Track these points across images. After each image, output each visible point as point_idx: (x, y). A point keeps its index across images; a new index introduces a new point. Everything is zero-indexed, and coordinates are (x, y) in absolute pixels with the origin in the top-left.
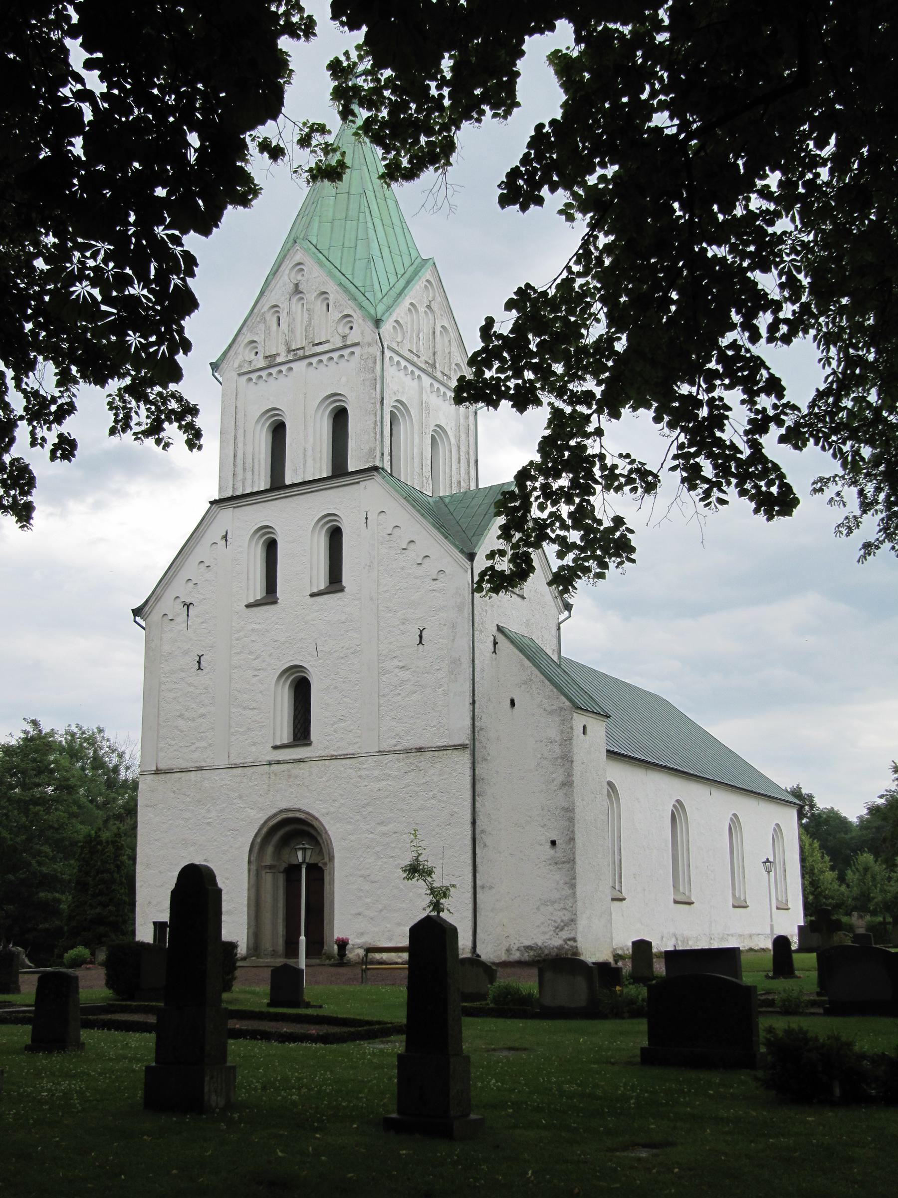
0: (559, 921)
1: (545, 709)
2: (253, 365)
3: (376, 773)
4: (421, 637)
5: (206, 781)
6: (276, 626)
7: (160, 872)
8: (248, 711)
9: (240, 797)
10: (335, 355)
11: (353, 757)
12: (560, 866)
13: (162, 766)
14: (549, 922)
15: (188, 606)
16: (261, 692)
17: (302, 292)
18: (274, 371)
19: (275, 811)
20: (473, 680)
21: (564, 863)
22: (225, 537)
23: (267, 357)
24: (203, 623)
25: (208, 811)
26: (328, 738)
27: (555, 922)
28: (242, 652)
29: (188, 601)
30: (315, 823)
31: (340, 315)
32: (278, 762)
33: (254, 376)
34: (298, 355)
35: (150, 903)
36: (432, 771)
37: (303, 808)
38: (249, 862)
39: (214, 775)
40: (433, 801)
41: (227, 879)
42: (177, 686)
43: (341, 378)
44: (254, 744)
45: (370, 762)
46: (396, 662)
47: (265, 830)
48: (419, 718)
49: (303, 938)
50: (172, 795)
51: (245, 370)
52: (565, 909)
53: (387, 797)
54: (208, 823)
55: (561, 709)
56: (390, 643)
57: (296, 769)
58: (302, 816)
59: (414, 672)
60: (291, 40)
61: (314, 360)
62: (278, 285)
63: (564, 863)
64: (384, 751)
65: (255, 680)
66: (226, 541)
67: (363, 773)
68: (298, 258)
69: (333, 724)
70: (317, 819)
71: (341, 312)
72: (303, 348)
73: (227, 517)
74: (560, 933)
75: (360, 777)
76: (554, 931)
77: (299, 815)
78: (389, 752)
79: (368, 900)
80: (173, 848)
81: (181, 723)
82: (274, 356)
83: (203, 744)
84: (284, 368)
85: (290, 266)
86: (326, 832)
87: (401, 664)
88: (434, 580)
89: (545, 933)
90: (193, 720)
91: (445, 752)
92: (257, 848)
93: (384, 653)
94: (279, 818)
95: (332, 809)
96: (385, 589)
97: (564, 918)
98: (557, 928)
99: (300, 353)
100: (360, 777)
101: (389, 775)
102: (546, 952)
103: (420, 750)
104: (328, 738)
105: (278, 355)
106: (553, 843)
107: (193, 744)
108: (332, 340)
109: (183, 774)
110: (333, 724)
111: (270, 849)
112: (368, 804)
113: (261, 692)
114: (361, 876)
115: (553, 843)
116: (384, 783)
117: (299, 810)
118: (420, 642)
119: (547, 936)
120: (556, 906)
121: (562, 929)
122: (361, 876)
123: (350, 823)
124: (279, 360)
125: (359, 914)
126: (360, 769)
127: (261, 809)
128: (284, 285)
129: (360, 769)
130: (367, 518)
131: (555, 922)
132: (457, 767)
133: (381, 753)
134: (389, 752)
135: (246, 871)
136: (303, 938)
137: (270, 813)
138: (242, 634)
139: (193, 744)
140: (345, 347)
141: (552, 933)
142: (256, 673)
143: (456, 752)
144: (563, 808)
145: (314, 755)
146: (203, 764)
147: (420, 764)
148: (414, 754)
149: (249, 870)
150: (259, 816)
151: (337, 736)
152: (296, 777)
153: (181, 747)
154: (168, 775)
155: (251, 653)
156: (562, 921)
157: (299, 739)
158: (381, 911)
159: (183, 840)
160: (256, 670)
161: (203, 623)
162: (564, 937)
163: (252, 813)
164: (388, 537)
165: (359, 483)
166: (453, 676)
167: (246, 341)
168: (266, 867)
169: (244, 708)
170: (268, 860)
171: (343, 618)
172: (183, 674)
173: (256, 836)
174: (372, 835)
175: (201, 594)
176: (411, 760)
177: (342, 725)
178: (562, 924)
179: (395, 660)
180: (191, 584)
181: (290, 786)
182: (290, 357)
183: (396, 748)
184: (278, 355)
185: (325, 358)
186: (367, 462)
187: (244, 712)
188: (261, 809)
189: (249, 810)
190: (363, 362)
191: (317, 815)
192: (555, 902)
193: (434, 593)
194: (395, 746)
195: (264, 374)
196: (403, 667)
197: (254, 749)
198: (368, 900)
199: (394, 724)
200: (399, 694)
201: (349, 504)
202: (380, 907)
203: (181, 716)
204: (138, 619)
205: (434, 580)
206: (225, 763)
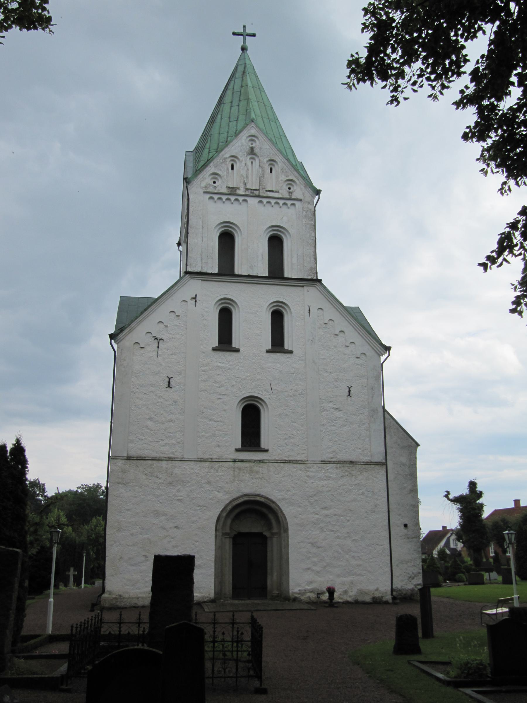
0: (411, 573)
1: (399, 445)
2: (217, 189)
3: (320, 475)
4: (349, 391)
5: (176, 469)
6: (238, 367)
7: (132, 535)
8: (213, 423)
9: (209, 483)
10: (281, 202)
11: (302, 462)
12: (410, 540)
13: (133, 453)
14: (405, 574)
15: (158, 340)
16: (225, 410)
17: (255, 154)
18: (233, 198)
19: (239, 495)
21: (413, 538)
22: (195, 298)
23: (229, 187)
24: (172, 354)
25: (178, 491)
26: (281, 448)
27: (408, 574)
28: (207, 380)
29: (159, 337)
30: (272, 505)
31: (287, 178)
32: (242, 461)
33: (216, 197)
34: (254, 194)
35: (121, 558)
36: (360, 477)
37: (263, 494)
38: (216, 530)
39: (185, 465)
40: (362, 496)
41: (197, 541)
42: (146, 396)
43: (284, 217)
44: (219, 446)
45: (315, 468)
46: (331, 405)
47: (230, 507)
48: (349, 442)
49: (83, 578)
50: (144, 477)
51: (209, 190)
52: (415, 566)
53: (329, 491)
54: (179, 500)
55: (409, 446)
56: (328, 392)
57: (257, 467)
58: (262, 500)
59: (345, 413)
61: (265, 201)
62: (237, 144)
63: (413, 538)
64: (324, 461)
65: (218, 401)
66: (196, 301)
67: (311, 474)
68: (253, 131)
69: (285, 439)
70: (273, 502)
71: (287, 176)
72: (259, 190)
73: (195, 286)
74: (412, 581)
75: (308, 476)
76: (408, 580)
77: (259, 499)
78: (330, 462)
79: (315, 559)
80: (144, 516)
81: (150, 423)
82: (235, 189)
83: (172, 441)
84: (241, 199)
85: (247, 135)
86: (282, 512)
87: (335, 406)
88: (358, 358)
89: (402, 581)
90: (163, 423)
91: (370, 466)
92: (222, 520)
93: (323, 398)
94: (241, 500)
96: (323, 357)
97: (413, 571)
98: (410, 577)
99: (257, 193)
100: (308, 476)
101: (330, 477)
102: (404, 592)
103: (352, 463)
104: (281, 448)
105: (239, 188)
106: (406, 526)
107: (163, 440)
108: (280, 191)
109: (155, 462)
110: (285, 439)
111: (229, 521)
112: (315, 495)
113: (225, 410)
114: (310, 543)
115: (406, 526)
116: (326, 482)
117: (259, 496)
118: (349, 395)
119: (404, 583)
120: (409, 564)
121: (413, 578)
122: (310, 543)
123: (300, 506)
124: (238, 192)
125: (308, 569)
126: (308, 471)
127: (227, 493)
128: (242, 145)
129: (308, 471)
130: (309, 310)
131: (408, 574)
132: (378, 476)
133: (323, 462)
134: (330, 462)
135: (214, 537)
136: (83, 578)
138: (207, 368)
139: (163, 440)
140: (290, 199)
141: (407, 580)
142: (220, 397)
143: (377, 467)
144: (411, 505)
145: (270, 458)
146: (173, 456)
147: (352, 472)
148: (348, 465)
149: (216, 536)
150: (226, 497)
151: (287, 447)
152: (257, 472)
153: (151, 442)
154: (140, 462)
155: (216, 382)
156: (413, 573)
157: (245, 446)
158: (325, 567)
159: (156, 511)
160: (220, 394)
161: (172, 354)
162: (414, 583)
163: (219, 495)
164: (324, 326)
165: (303, 286)
166: (373, 419)
167: (211, 172)
169: (210, 420)
170: (228, 530)
171: (292, 371)
172: (153, 389)
173: (222, 511)
174: (317, 516)
175: (171, 334)
176: (346, 469)
177: (292, 440)
178: (413, 575)
179: (331, 403)
180: (162, 326)
181: (252, 478)
182: (248, 193)
183: (332, 460)
184: (239, 188)
185: (273, 201)
186: (309, 275)
187: (210, 423)
188: (227, 493)
189: (217, 493)
190: (304, 212)
191: (274, 500)
192: (408, 562)
193: (357, 366)
194: (332, 458)
195: (224, 198)
196: (337, 409)
197: (218, 449)
198: (315, 559)
199: (331, 444)
200: (334, 425)
201: (294, 299)
202: (325, 564)
203: (151, 419)
204: (113, 341)
205: (358, 358)
206: (194, 457)
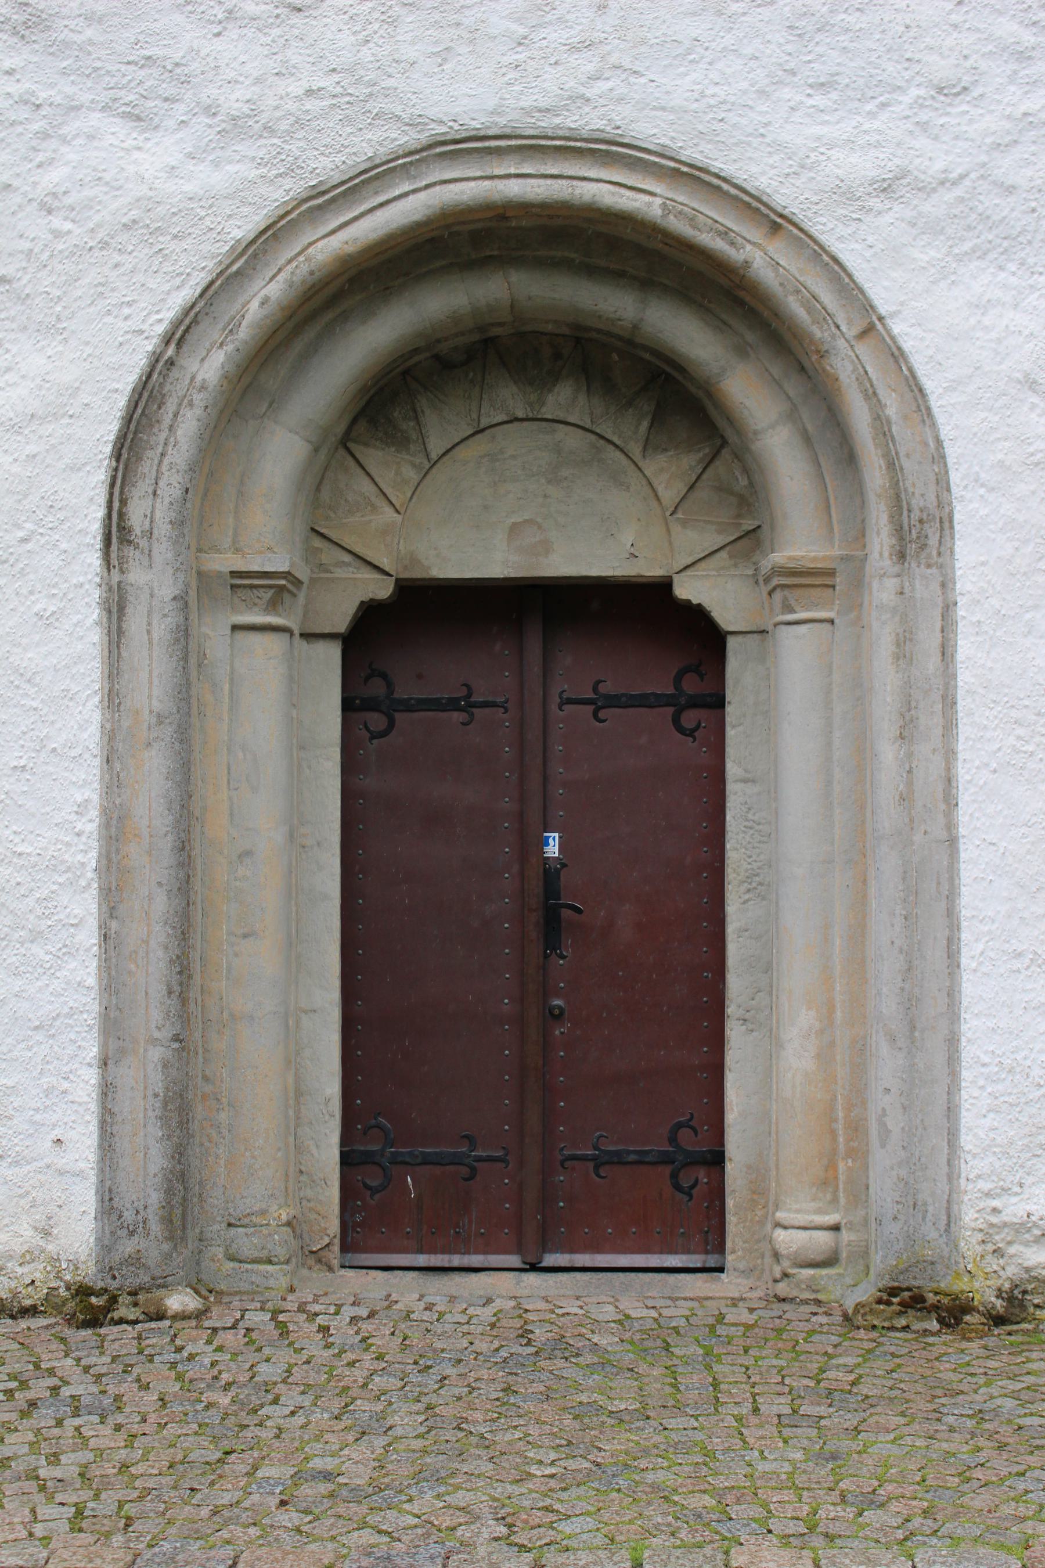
19: (370, 143)
20: (704, 558)
37: (649, 130)
38: (116, 534)
58: (647, 200)
60: (690, 597)
70: (776, 223)
86: (872, 327)
92: (183, 431)
95: (934, 158)
111: (281, 451)
127: (236, 127)
137: (327, 163)
149: (116, 606)
150: (205, 178)
168: (242, 582)
170: (264, 534)
173: (181, 333)
188: (236, 127)
191: (786, 195)
